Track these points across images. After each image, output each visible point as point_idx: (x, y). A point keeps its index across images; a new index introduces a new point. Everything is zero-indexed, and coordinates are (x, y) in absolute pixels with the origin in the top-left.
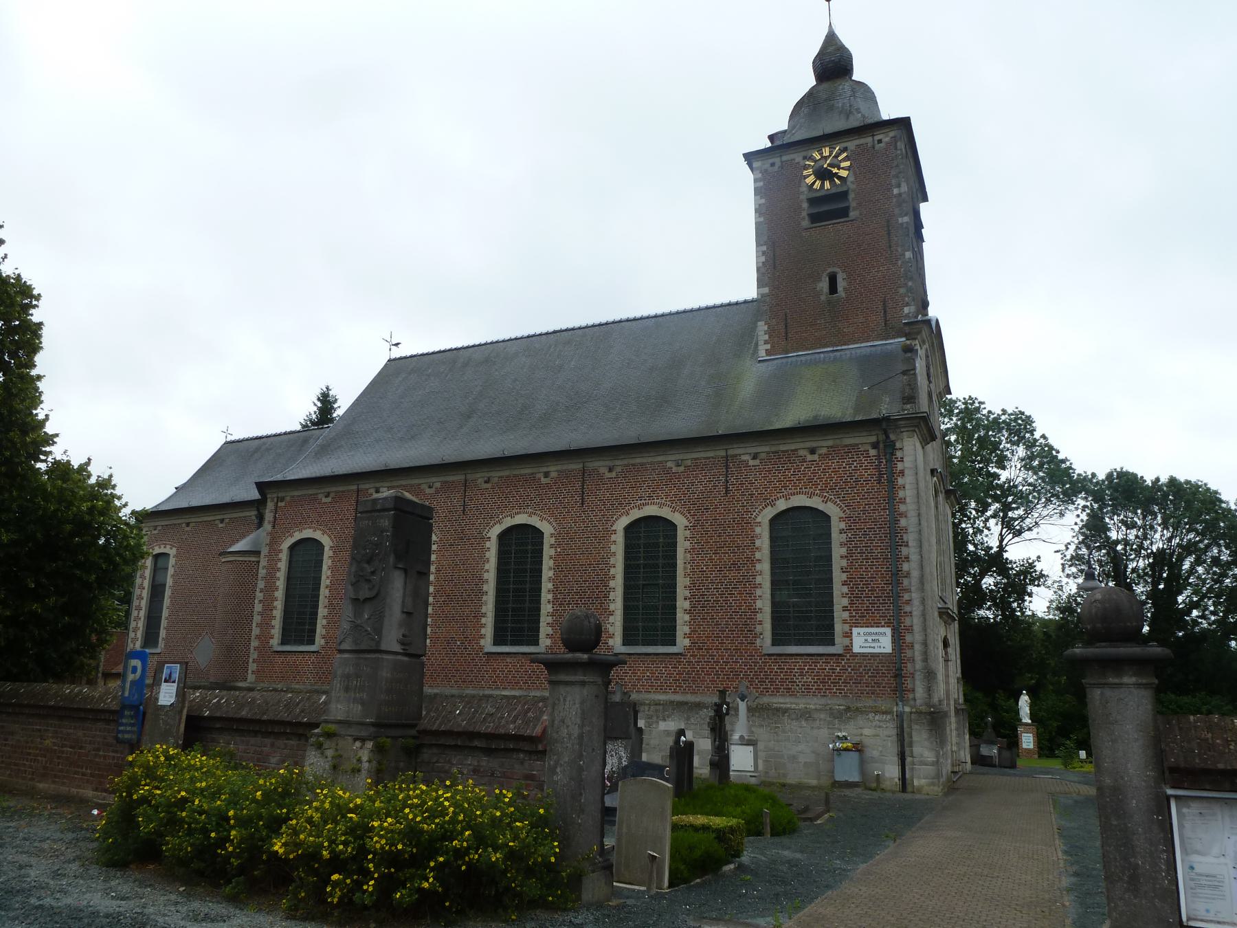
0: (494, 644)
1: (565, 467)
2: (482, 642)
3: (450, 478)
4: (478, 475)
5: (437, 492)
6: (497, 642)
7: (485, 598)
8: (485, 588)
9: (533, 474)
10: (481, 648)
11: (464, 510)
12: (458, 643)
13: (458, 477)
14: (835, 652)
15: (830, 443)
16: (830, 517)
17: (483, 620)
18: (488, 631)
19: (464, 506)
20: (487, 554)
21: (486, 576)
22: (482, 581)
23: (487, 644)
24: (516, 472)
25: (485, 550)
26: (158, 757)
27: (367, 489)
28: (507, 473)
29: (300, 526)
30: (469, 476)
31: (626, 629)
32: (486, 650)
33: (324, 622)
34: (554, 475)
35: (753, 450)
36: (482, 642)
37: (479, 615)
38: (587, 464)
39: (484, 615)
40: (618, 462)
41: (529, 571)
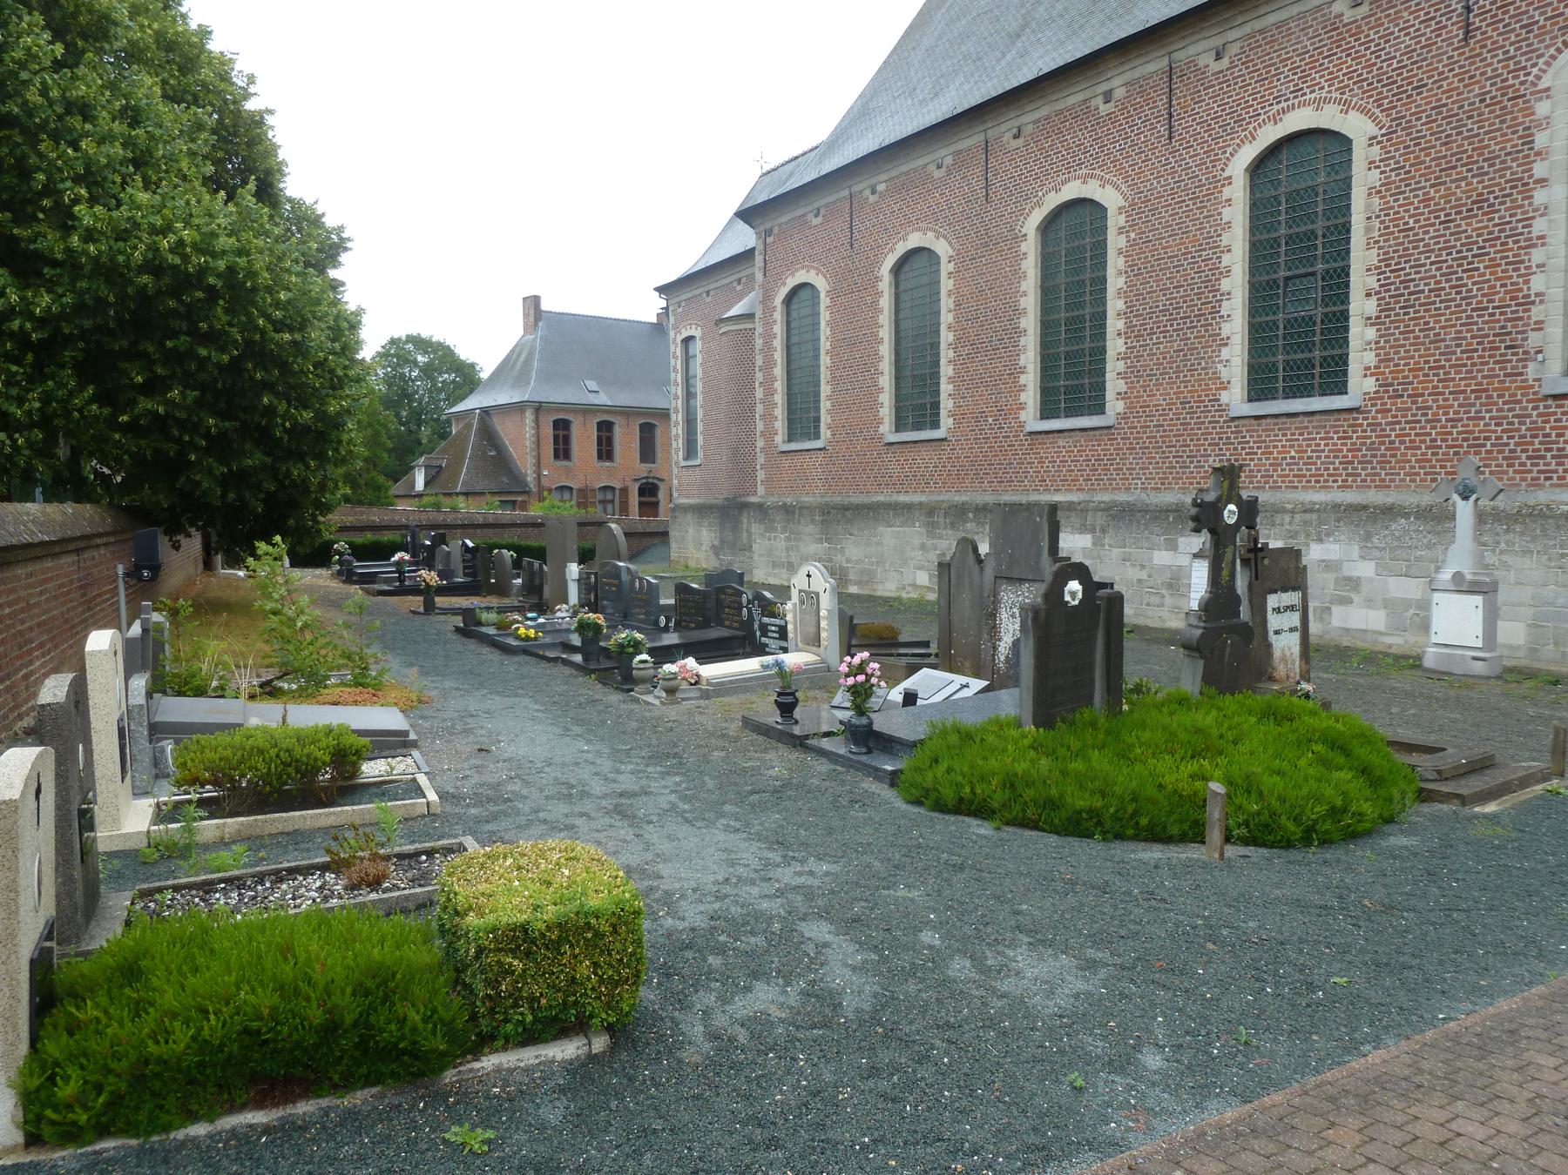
0: (1042, 418)
1: (1137, 74)
2: (1224, 397)
6: (1044, 416)
10: (1222, 409)
11: (987, 194)
12: (990, 420)
13: (1151, 66)
18: (1030, 397)
23: (1030, 418)
24: (1060, 105)
28: (1044, 112)
29: (790, 267)
32: (1028, 429)
35: (1217, 42)
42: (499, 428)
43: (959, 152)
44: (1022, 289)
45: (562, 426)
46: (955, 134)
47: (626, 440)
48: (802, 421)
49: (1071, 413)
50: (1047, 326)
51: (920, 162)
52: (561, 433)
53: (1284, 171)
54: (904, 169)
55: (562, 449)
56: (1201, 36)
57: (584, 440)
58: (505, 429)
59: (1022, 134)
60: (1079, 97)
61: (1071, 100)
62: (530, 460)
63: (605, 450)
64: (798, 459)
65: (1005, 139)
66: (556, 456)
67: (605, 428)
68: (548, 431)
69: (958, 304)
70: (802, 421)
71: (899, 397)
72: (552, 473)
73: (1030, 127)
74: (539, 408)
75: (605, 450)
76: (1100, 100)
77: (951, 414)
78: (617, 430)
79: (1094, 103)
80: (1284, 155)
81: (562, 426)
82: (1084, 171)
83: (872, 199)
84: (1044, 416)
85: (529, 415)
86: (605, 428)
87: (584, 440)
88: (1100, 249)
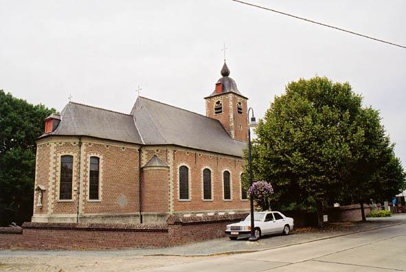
64: (183, 203)
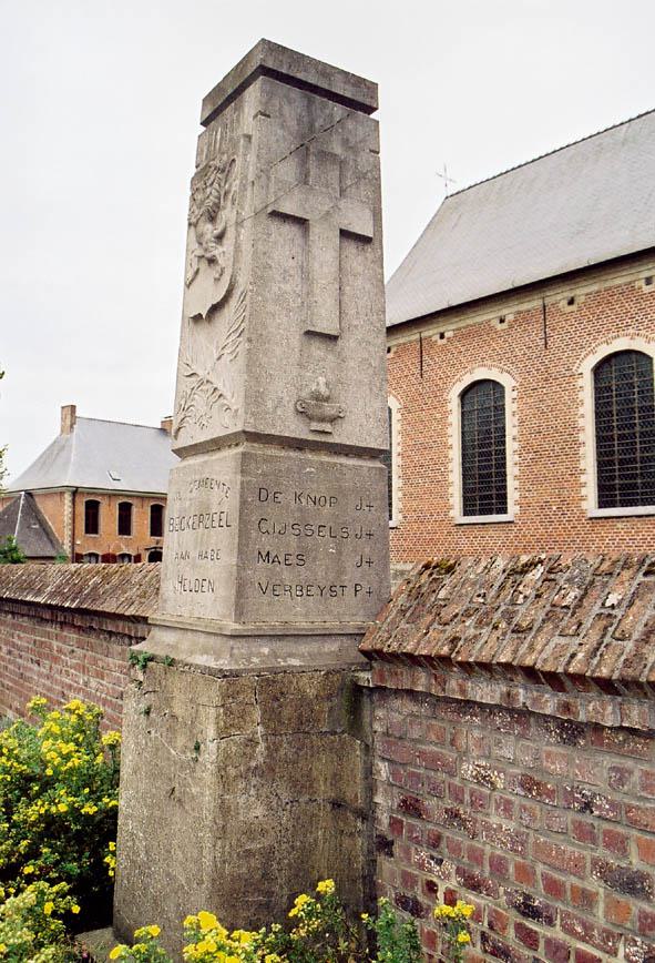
0: (600, 507)
1: (462, 324)
2: (584, 505)
3: (525, 306)
4: (559, 297)
5: (511, 327)
6: (602, 504)
7: (582, 450)
8: (582, 437)
9: (630, 283)
10: (583, 512)
11: (546, 343)
12: (554, 508)
13: (533, 303)
14: (508, 520)
15: (454, 327)
16: (651, 359)
17: (583, 479)
18: (590, 491)
19: (545, 339)
20: (581, 395)
21: (581, 422)
22: (576, 429)
23: (591, 506)
24: (608, 284)
25: (576, 390)
26: (242, 654)
27: (430, 337)
28: (595, 288)
29: (505, 359)
30: (547, 301)
31: (601, 488)
32: (590, 515)
33: (400, 494)
34: (510, 318)
35: (569, 295)
36: (584, 505)
37: (576, 473)
38: (547, 301)
39: (583, 472)
40: (578, 292)
41: (637, 410)
42: (40, 506)
43: (519, 313)
44: (580, 413)
45: (92, 509)
46: (526, 296)
47: (141, 518)
48: (485, 491)
49: (483, 512)
50: (602, 439)
51: (485, 317)
52: (91, 511)
53: (613, 372)
54: (470, 322)
55: (92, 526)
56: (620, 274)
57: (109, 517)
58: (46, 508)
59: (576, 302)
60: (628, 279)
61: (618, 281)
62: (68, 532)
63: (125, 528)
65: (560, 305)
66: (87, 532)
67: (125, 510)
68: (81, 509)
69: (522, 422)
70: (485, 491)
71: (466, 490)
72: (85, 544)
73: (583, 297)
74: (75, 492)
75: (125, 528)
76: (642, 283)
77: (517, 503)
78: (134, 510)
79: (637, 284)
80: (613, 361)
81: (92, 509)
82: (631, 331)
83: (440, 342)
84: (602, 504)
85: (68, 498)
86: (125, 510)
87: (109, 517)
88: (501, 409)
